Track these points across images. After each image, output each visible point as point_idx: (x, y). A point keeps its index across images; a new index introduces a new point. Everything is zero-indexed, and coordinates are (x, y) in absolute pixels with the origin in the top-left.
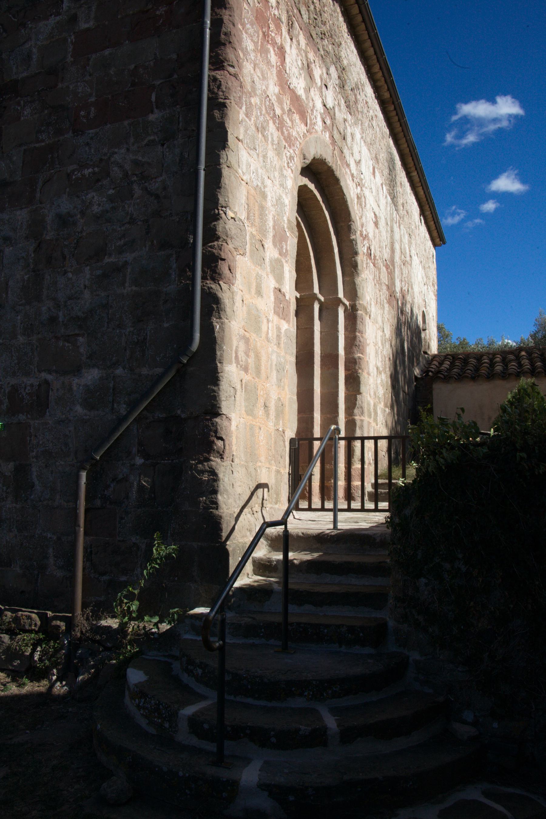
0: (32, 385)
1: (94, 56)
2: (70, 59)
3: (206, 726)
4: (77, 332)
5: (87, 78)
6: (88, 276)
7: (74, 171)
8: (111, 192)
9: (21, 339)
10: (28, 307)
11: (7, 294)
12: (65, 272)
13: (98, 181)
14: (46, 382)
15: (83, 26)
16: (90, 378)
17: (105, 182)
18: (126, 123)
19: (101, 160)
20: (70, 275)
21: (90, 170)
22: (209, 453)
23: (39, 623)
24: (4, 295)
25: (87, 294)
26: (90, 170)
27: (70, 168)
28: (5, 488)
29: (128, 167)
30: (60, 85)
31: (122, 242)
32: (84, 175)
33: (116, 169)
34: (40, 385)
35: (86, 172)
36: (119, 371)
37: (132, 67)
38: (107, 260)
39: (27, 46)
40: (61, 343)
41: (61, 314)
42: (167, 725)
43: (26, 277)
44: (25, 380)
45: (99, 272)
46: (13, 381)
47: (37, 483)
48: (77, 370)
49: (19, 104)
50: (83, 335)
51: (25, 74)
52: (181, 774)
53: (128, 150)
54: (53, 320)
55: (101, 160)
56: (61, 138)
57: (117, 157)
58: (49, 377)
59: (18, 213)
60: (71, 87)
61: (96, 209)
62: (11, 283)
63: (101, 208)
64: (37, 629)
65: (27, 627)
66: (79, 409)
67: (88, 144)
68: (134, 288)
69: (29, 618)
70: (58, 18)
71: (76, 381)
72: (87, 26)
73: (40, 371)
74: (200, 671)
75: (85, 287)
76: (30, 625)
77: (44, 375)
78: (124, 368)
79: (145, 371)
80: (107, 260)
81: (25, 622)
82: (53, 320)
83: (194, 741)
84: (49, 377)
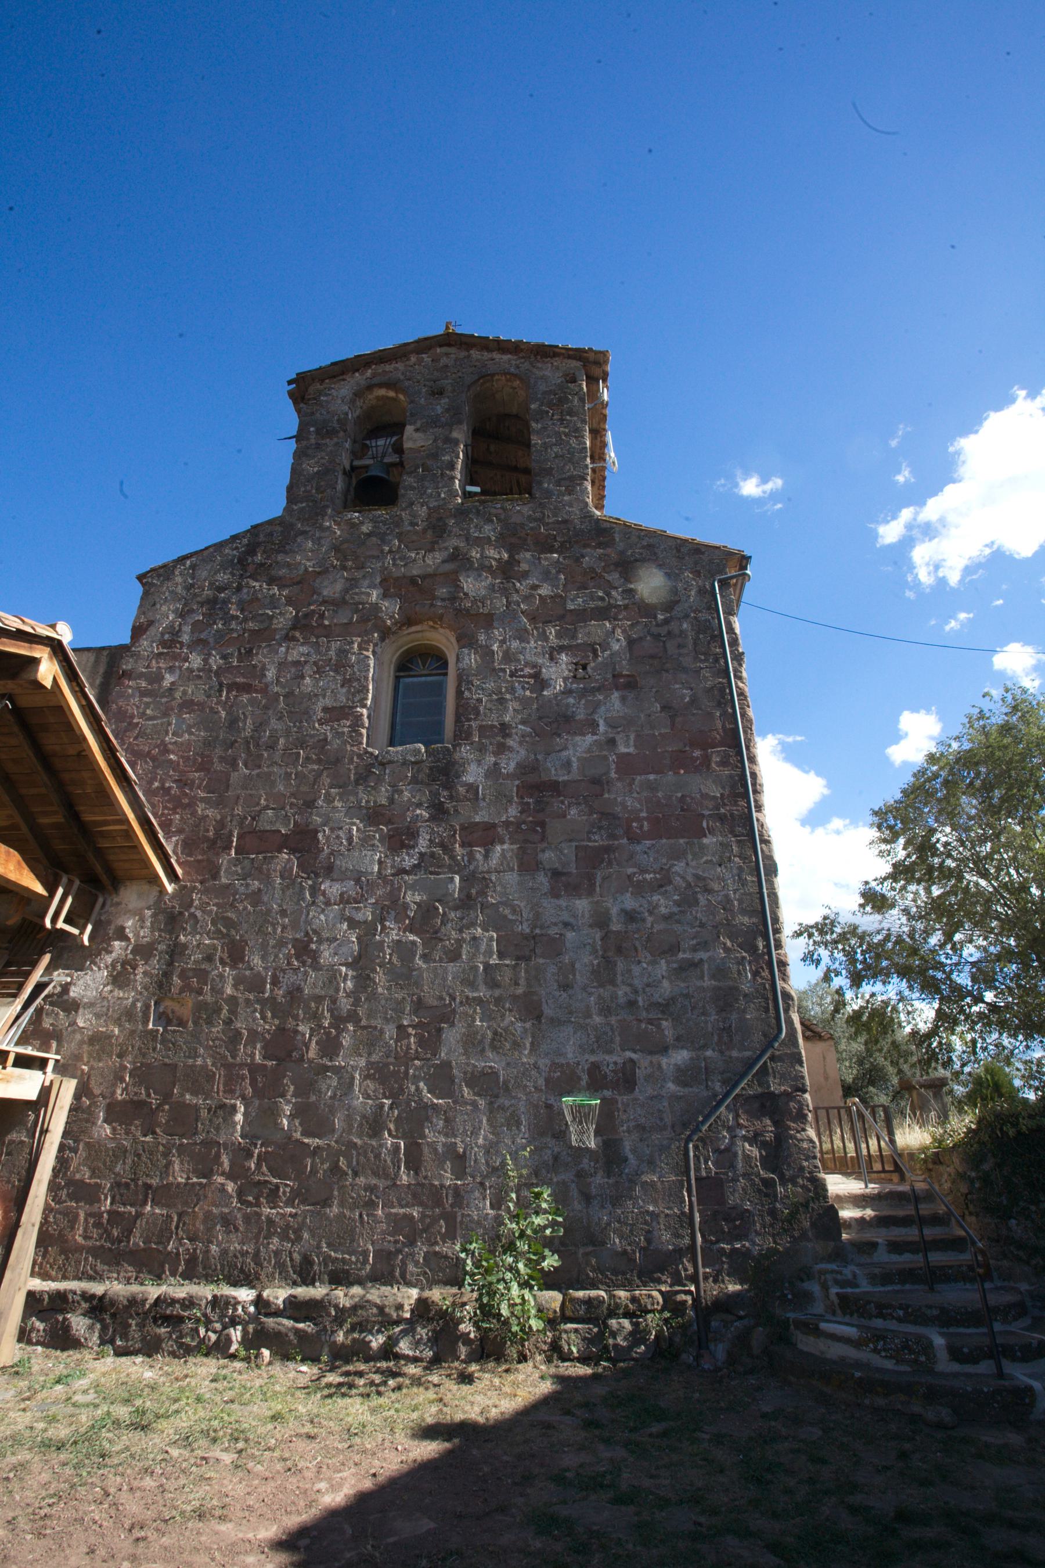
0: (615, 1063)
1: (639, 778)
2: (613, 775)
3: (965, 1350)
4: (660, 1016)
5: (635, 795)
6: (664, 968)
7: (635, 873)
8: (676, 897)
9: (597, 1019)
10: (602, 990)
11: (574, 975)
12: (639, 962)
13: (661, 886)
14: (632, 1060)
15: (623, 749)
16: (679, 1058)
17: (669, 888)
18: (682, 841)
19: (662, 869)
20: (645, 965)
21: (652, 876)
22: (805, 1124)
23: (661, 1300)
24: (571, 977)
25: (666, 983)
26: (652, 876)
27: (630, 871)
28: (592, 1164)
29: (690, 878)
30: (606, 796)
31: (694, 942)
32: (645, 879)
33: (678, 878)
34: (624, 1063)
35: (648, 877)
36: (709, 1053)
37: (679, 795)
38: (681, 955)
39: (565, 753)
40: (643, 1026)
41: (640, 999)
42: (923, 1359)
43: (595, 962)
44: (607, 1058)
45: (675, 965)
46: (593, 1058)
47: (631, 1156)
48: (664, 1050)
49: (562, 802)
50: (667, 1020)
51: (566, 778)
52: (985, 1390)
53: (687, 864)
54: (632, 1004)
55: (662, 869)
56: (616, 842)
57: (676, 869)
58: (634, 1056)
59: (578, 902)
60: (619, 799)
61: (663, 910)
62: (577, 966)
63: (668, 910)
64: (659, 1308)
65: (649, 1307)
66: (671, 1086)
67: (645, 853)
68: (713, 982)
69: (650, 1296)
70: (595, 737)
71: (664, 1061)
72: (626, 750)
73: (623, 1050)
74: (901, 1313)
75: (663, 977)
76: (653, 1304)
77: (629, 1054)
78: (714, 1050)
79: (735, 1054)
80: (681, 955)
81: (644, 1301)
82: (632, 1004)
83: (956, 1367)
84: (634, 1056)
